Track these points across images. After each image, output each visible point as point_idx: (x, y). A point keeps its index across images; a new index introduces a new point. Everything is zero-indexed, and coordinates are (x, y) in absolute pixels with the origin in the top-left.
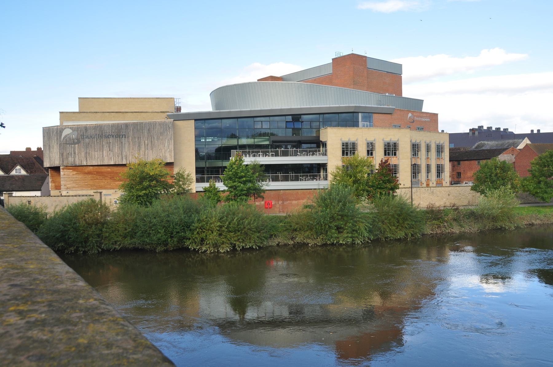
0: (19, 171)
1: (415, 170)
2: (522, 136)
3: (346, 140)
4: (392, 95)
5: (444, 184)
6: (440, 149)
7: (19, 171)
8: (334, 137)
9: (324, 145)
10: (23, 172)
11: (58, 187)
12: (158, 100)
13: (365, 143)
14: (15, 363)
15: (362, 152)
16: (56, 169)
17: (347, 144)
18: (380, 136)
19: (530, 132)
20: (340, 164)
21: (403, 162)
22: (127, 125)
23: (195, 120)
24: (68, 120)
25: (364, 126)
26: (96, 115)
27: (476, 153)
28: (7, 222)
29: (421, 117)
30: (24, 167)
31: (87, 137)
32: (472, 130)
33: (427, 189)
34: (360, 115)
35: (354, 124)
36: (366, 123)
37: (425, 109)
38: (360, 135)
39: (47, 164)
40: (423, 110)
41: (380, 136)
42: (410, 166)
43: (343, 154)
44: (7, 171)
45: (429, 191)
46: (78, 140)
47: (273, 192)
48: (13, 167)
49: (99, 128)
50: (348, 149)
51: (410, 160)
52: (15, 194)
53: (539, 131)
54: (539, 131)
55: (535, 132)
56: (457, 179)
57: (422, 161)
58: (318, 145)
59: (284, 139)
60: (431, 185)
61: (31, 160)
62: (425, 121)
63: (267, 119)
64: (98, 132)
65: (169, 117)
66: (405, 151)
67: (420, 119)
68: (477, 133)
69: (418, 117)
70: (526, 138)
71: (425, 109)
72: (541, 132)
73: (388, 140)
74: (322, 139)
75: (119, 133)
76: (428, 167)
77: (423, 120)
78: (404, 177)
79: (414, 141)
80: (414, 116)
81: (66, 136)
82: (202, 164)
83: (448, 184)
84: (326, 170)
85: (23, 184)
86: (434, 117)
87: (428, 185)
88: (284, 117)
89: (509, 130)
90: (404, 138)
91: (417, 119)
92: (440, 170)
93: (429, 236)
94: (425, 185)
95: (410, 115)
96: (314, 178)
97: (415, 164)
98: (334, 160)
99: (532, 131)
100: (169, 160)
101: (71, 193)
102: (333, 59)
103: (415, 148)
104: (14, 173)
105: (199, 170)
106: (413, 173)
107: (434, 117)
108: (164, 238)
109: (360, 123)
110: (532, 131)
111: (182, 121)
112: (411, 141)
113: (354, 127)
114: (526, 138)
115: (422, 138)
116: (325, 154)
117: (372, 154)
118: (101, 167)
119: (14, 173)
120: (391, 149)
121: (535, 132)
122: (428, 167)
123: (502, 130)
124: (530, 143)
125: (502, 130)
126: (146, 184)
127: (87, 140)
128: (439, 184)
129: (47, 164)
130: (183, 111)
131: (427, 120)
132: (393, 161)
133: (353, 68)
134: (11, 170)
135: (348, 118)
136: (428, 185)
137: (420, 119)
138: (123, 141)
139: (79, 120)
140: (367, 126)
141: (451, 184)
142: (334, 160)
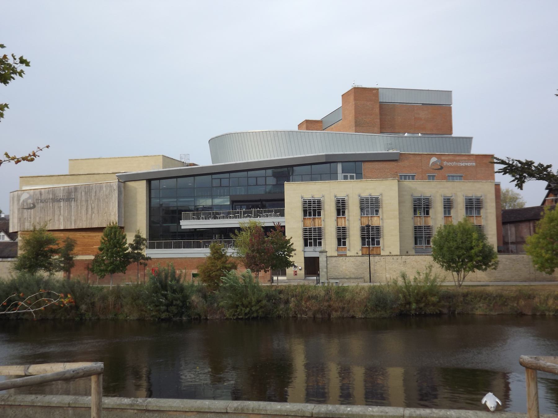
3: (308, 197)
4: (416, 135)
5: (308, 248)
8: (295, 193)
12: (146, 158)
17: (419, 199)
22: (76, 188)
24: (28, 184)
26: (52, 178)
29: (458, 161)
31: (41, 201)
35: (332, 176)
36: (349, 175)
37: (476, 150)
38: (326, 191)
41: (352, 190)
43: (305, 215)
46: (34, 204)
49: (53, 191)
50: (312, 209)
59: (246, 199)
62: (466, 167)
63: (227, 175)
64: (51, 196)
75: (70, 196)
77: (463, 164)
80: (444, 160)
81: (23, 201)
88: (264, 171)
97: (368, 226)
109: (340, 175)
111: (133, 182)
113: (312, 180)
116: (282, 214)
118: (54, 232)
127: (42, 204)
132: (375, 222)
135: (321, 168)
139: (37, 184)
140: (352, 178)
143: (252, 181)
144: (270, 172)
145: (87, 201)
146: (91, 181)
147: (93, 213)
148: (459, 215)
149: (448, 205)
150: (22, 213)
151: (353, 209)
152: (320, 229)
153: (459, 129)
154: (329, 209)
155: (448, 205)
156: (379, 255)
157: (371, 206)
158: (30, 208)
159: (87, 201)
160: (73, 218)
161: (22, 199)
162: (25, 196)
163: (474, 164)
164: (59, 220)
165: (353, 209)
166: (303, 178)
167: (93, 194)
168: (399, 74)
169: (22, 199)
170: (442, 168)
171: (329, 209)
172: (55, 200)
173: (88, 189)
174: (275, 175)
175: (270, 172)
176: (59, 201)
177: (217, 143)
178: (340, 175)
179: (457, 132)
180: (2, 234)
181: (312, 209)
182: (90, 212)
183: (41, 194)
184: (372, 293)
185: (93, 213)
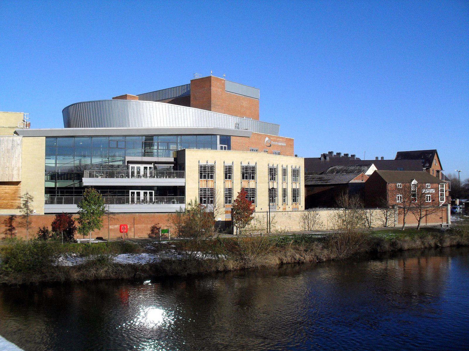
1: (272, 193)
2: (368, 164)
6: (295, 173)
8: (194, 158)
14: (116, 350)
19: (375, 159)
21: (261, 185)
23: (47, 137)
25: (222, 148)
29: (278, 141)
32: (324, 156)
33: (284, 213)
35: (213, 146)
36: (224, 146)
41: (237, 158)
42: (267, 190)
45: (286, 215)
47: (128, 215)
50: (206, 172)
51: (267, 184)
53: (382, 158)
54: (382, 158)
55: (380, 159)
57: (279, 185)
60: (287, 209)
62: (282, 146)
66: (262, 174)
68: (328, 158)
69: (275, 141)
70: (373, 165)
72: (385, 159)
73: (245, 164)
76: (285, 191)
77: (280, 144)
79: (271, 165)
80: (272, 140)
89: (357, 157)
91: (274, 143)
92: (295, 193)
95: (267, 139)
99: (377, 158)
103: (272, 172)
106: (293, 197)
108: (29, 263)
109: (219, 146)
110: (377, 158)
112: (268, 165)
114: (373, 165)
120: (249, 173)
122: (285, 191)
123: (350, 156)
124: (376, 169)
125: (350, 156)
131: (283, 144)
140: (225, 148)
144: (144, 138)
151: (237, 173)
154: (219, 173)
157: (249, 173)
165: (237, 173)
170: (270, 146)
171: (219, 173)
178: (219, 146)
181: (206, 172)
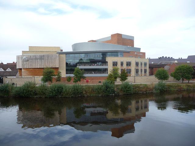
0: (9, 70)
1: (137, 71)
3: (114, 61)
6: (145, 64)
7: (9, 70)
8: (110, 60)
9: (107, 62)
10: (10, 70)
11: (21, 75)
13: (126, 62)
15: (119, 66)
16: (21, 69)
18: (125, 60)
20: (112, 69)
21: (133, 68)
22: (44, 56)
27: (157, 68)
28: (56, 77)
30: (11, 68)
31: (31, 59)
34: (119, 53)
35: (117, 56)
37: (141, 51)
38: (115, 59)
39: (18, 67)
40: (141, 52)
41: (125, 60)
44: (5, 70)
48: (7, 68)
49: (35, 56)
50: (115, 64)
52: (8, 77)
53: (181, 58)
54: (181, 58)
55: (180, 58)
56: (151, 74)
57: (139, 68)
58: (104, 62)
61: (13, 66)
64: (34, 58)
65: (57, 53)
67: (139, 54)
69: (138, 53)
71: (141, 51)
74: (106, 61)
75: (42, 58)
76: (141, 70)
78: (133, 73)
82: (68, 68)
83: (148, 75)
84: (107, 70)
85: (11, 74)
86: (144, 54)
87: (141, 76)
88: (99, 53)
90: (133, 60)
93: (140, 95)
94: (140, 76)
95: (136, 53)
96: (103, 73)
98: (110, 67)
99: (179, 58)
100: (57, 67)
101: (25, 77)
102: (111, 35)
103: (137, 64)
104: (7, 70)
105: (67, 70)
107: (144, 54)
110: (179, 58)
115: (139, 60)
117: (122, 65)
119: (7, 70)
120: (129, 64)
121: (180, 58)
122: (141, 70)
126: (49, 74)
128: (145, 75)
129: (18, 67)
130: (63, 51)
133: (119, 38)
134: (6, 69)
135: (115, 53)
136: (141, 76)
137: (139, 54)
138: (43, 60)
141: (149, 75)
142: (110, 67)
143: (96, 56)
144: (101, 54)
145: (48, 60)
146: (48, 54)
147: (50, 63)
148: (125, 66)
149: (122, 64)
150: (23, 62)
152: (130, 69)
153: (136, 46)
155: (122, 64)
156: (130, 76)
158: (27, 61)
159: (48, 60)
160: (43, 65)
161: (23, 58)
162: (24, 57)
163: (142, 54)
164: (38, 65)
166: (112, 55)
167: (50, 58)
168: (125, 32)
169: (23, 58)
172: (36, 59)
173: (48, 56)
174: (102, 55)
175: (101, 54)
176: (37, 59)
177: (75, 46)
179: (135, 46)
180: (1, 68)
182: (49, 62)
183: (31, 57)
184: (28, 87)
185: (50, 63)
